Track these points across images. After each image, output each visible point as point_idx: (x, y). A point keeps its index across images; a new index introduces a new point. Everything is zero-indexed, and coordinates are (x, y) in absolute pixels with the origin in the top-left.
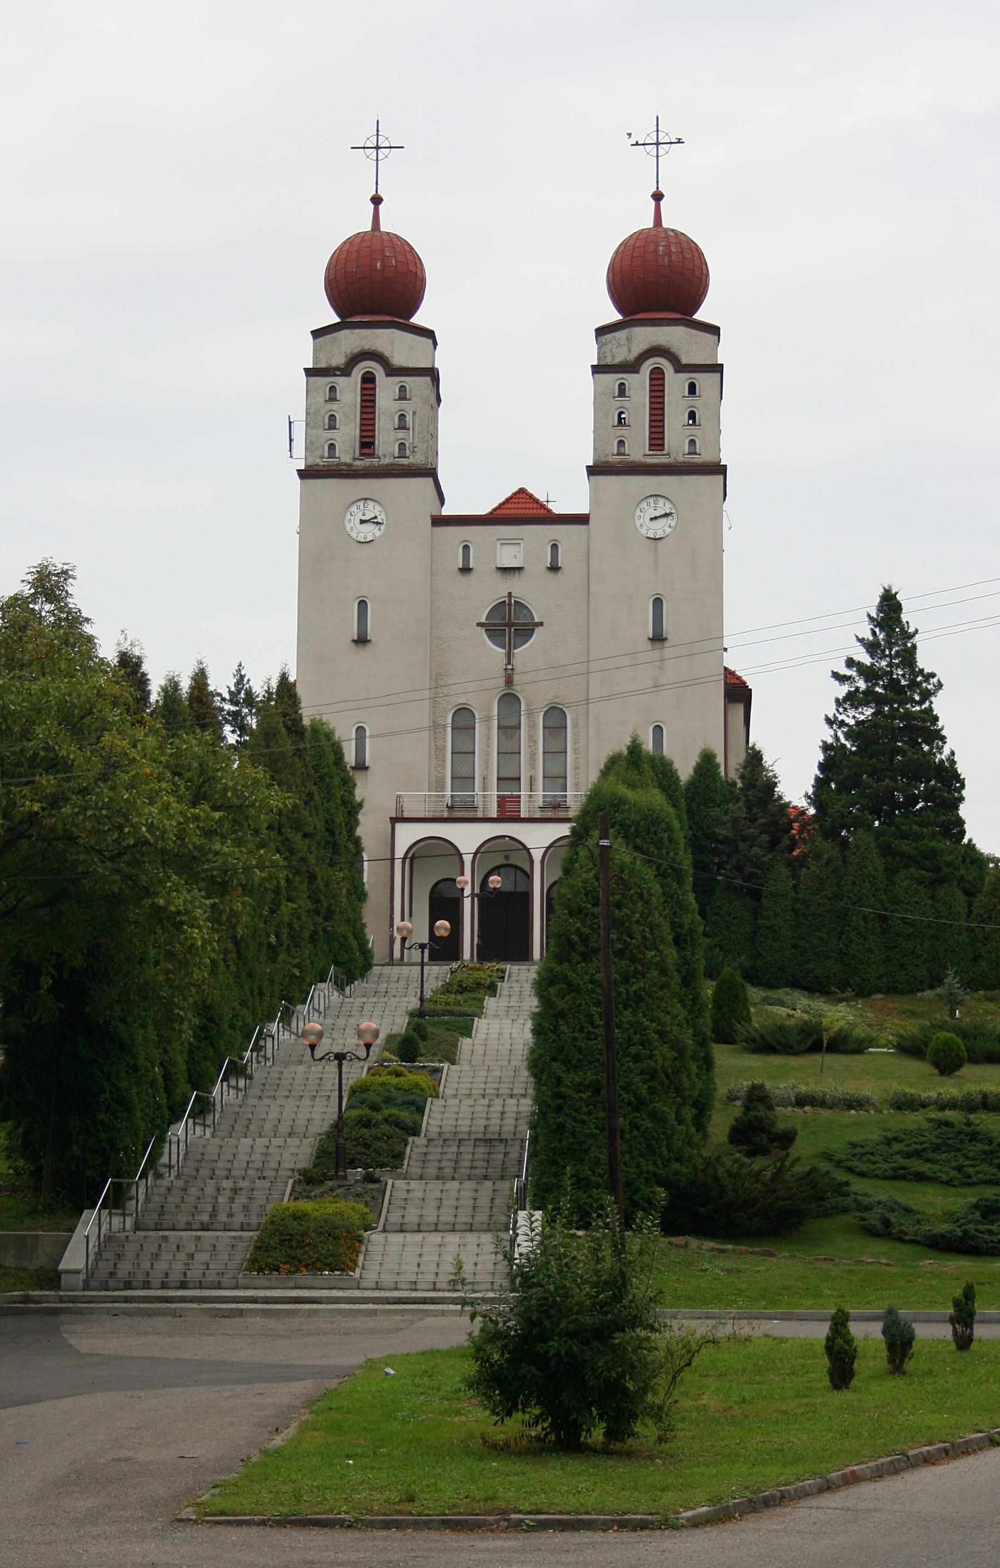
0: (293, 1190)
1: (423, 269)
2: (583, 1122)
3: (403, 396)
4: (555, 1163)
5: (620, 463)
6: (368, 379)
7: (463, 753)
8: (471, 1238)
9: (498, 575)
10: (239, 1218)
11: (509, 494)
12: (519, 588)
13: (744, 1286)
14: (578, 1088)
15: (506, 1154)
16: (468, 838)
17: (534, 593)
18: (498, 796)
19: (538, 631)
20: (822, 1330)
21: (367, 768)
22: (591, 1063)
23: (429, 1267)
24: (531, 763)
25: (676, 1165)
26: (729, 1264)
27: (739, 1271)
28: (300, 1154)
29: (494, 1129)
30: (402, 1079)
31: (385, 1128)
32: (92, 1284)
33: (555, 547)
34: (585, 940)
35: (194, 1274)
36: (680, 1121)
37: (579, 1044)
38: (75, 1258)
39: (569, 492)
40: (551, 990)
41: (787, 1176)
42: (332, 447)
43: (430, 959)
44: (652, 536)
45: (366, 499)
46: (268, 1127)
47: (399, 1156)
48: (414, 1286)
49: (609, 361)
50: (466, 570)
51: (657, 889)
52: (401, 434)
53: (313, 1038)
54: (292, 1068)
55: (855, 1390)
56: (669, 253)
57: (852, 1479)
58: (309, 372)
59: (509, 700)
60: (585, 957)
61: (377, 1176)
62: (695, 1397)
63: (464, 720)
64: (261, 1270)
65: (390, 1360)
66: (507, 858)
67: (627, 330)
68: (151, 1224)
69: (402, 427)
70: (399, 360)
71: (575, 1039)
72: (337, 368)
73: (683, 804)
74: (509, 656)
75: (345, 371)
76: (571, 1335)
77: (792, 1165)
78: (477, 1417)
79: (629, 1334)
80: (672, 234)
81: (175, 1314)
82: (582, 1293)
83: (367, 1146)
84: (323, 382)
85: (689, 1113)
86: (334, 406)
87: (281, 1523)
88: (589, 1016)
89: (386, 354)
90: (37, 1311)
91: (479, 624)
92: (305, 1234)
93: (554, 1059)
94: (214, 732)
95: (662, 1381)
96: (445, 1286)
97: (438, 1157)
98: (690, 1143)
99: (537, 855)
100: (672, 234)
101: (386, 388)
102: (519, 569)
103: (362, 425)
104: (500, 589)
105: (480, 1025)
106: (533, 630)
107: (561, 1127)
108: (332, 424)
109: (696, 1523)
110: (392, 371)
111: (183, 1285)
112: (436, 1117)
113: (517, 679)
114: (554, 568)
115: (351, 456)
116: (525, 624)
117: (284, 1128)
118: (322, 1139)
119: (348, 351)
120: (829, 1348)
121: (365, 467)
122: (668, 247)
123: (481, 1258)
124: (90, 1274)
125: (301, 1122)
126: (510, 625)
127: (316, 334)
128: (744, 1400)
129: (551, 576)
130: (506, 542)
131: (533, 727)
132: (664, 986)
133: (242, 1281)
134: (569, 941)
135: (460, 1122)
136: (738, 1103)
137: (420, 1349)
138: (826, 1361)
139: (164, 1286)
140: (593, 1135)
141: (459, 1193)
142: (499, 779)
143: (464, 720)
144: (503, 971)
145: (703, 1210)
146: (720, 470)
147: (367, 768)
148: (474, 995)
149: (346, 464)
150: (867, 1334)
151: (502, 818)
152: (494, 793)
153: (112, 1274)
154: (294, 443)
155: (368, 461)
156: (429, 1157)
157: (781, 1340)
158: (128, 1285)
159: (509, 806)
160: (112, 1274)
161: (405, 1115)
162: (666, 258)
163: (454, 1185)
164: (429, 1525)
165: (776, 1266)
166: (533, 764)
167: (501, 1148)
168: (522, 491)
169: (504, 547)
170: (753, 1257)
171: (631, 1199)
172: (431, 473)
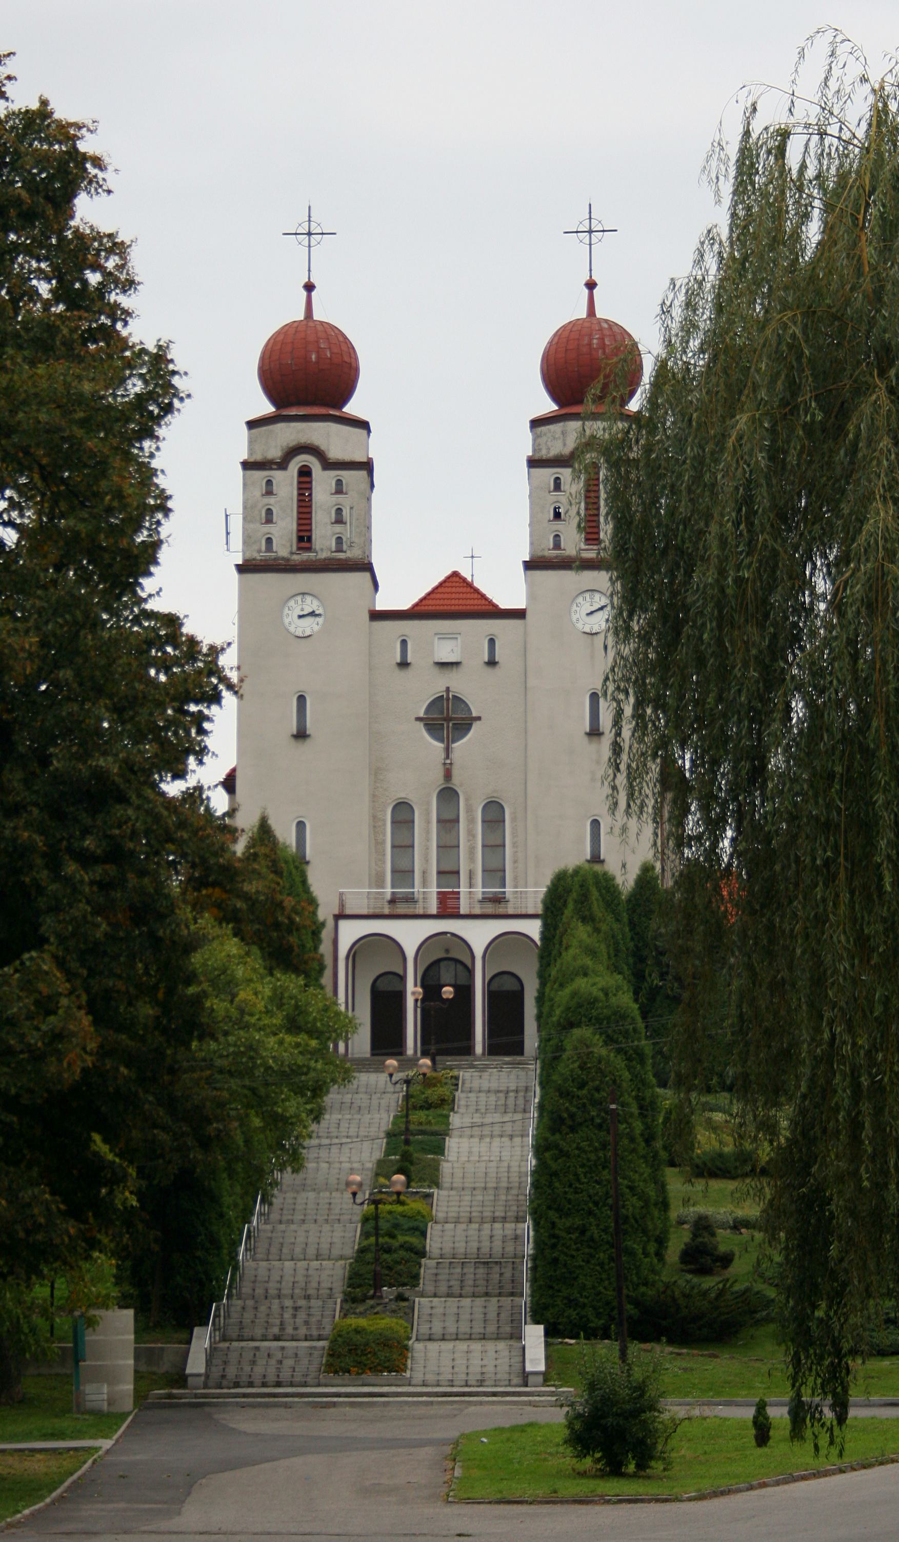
0: (341, 1308)
1: (356, 359)
2: (573, 1257)
3: (339, 489)
4: (551, 1287)
5: (556, 557)
6: (305, 473)
7: (403, 847)
8: (490, 1346)
9: (436, 670)
10: (303, 1331)
11: (442, 578)
12: (458, 683)
13: (696, 1381)
14: (569, 1231)
15: (501, 1274)
16: (410, 935)
17: (471, 686)
18: (439, 893)
19: (476, 726)
20: (749, 1413)
22: (578, 1211)
23: (461, 1368)
24: (471, 857)
25: (643, 1289)
26: (684, 1365)
27: (692, 1370)
28: (333, 1275)
29: (485, 1250)
30: (406, 1207)
31: (402, 1253)
32: (210, 1384)
33: (492, 642)
34: (572, 1116)
35: (285, 1375)
36: (646, 1255)
37: (568, 1196)
38: (196, 1364)
39: (506, 586)
40: (547, 1155)
41: (728, 1296)
42: (269, 541)
44: (588, 631)
45: (303, 594)
46: (298, 1250)
47: (416, 1277)
48: (451, 1383)
49: (544, 454)
50: (404, 664)
51: (627, 1075)
52: (338, 528)
53: (354, 1188)
54: (304, 1195)
55: (771, 1447)
56: (603, 346)
57: (764, 1485)
58: (246, 465)
59: (448, 795)
60: (573, 1129)
61: (406, 1296)
62: (680, 1450)
63: (403, 814)
64: (336, 1372)
65: (485, 1433)
66: (447, 951)
67: (561, 424)
68: (234, 1335)
69: (339, 521)
70: (335, 453)
71: (566, 1193)
72: (276, 463)
73: (625, 917)
74: (448, 750)
75: (282, 465)
76: (617, 1415)
77: (731, 1286)
78: (567, 1460)
79: (648, 1414)
80: (606, 326)
81: (286, 1406)
82: (624, 1393)
83: (390, 1268)
84: (260, 476)
85: (652, 1248)
86: (271, 500)
87: (499, 1502)
88: (576, 1175)
89: (322, 448)
90: (184, 1404)
91: (418, 719)
92: (367, 1344)
93: (549, 1208)
95: (661, 1441)
96: (474, 1383)
97: (446, 1277)
98: (653, 1271)
99: (478, 951)
100: (606, 326)
101: (323, 481)
102: (457, 664)
103: (299, 519)
104: (438, 684)
105: (452, 1144)
106: (471, 725)
107: (555, 1261)
108: (269, 517)
109: (690, 1499)
110: (329, 465)
111: (278, 1384)
112: (437, 1240)
113: (455, 772)
114: (492, 663)
115: (289, 550)
116: (463, 719)
117: (311, 1251)
118: (351, 1264)
119: (285, 444)
120: (755, 1422)
121: (303, 562)
122: (602, 339)
123: (499, 1362)
124: (207, 1376)
125: (325, 1246)
126: (448, 719)
127: (252, 424)
128: (705, 1453)
129: (489, 670)
130: (444, 636)
131: (471, 820)
132: (634, 1150)
133: (323, 1381)
134: (560, 1118)
135: (457, 1245)
136: (686, 1226)
137: (493, 1426)
138: (753, 1432)
139: (264, 1385)
140: (580, 1267)
141: (471, 1309)
142: (439, 873)
143: (403, 814)
144: (457, 1078)
145: (664, 1323)
148: (439, 1111)
149: (283, 558)
150: (779, 1414)
151: (442, 915)
152: (434, 890)
153: (223, 1377)
154: (231, 536)
155: (305, 556)
156: (440, 1277)
157: (726, 1419)
158: (237, 1385)
159: (450, 903)
160: (223, 1377)
161: (413, 1240)
162: (600, 352)
163: (466, 1302)
164: (567, 1502)
165: (721, 1365)
166: (472, 859)
167: (496, 1269)
168: (455, 574)
169: (442, 642)
170: (701, 1359)
171: (610, 1316)
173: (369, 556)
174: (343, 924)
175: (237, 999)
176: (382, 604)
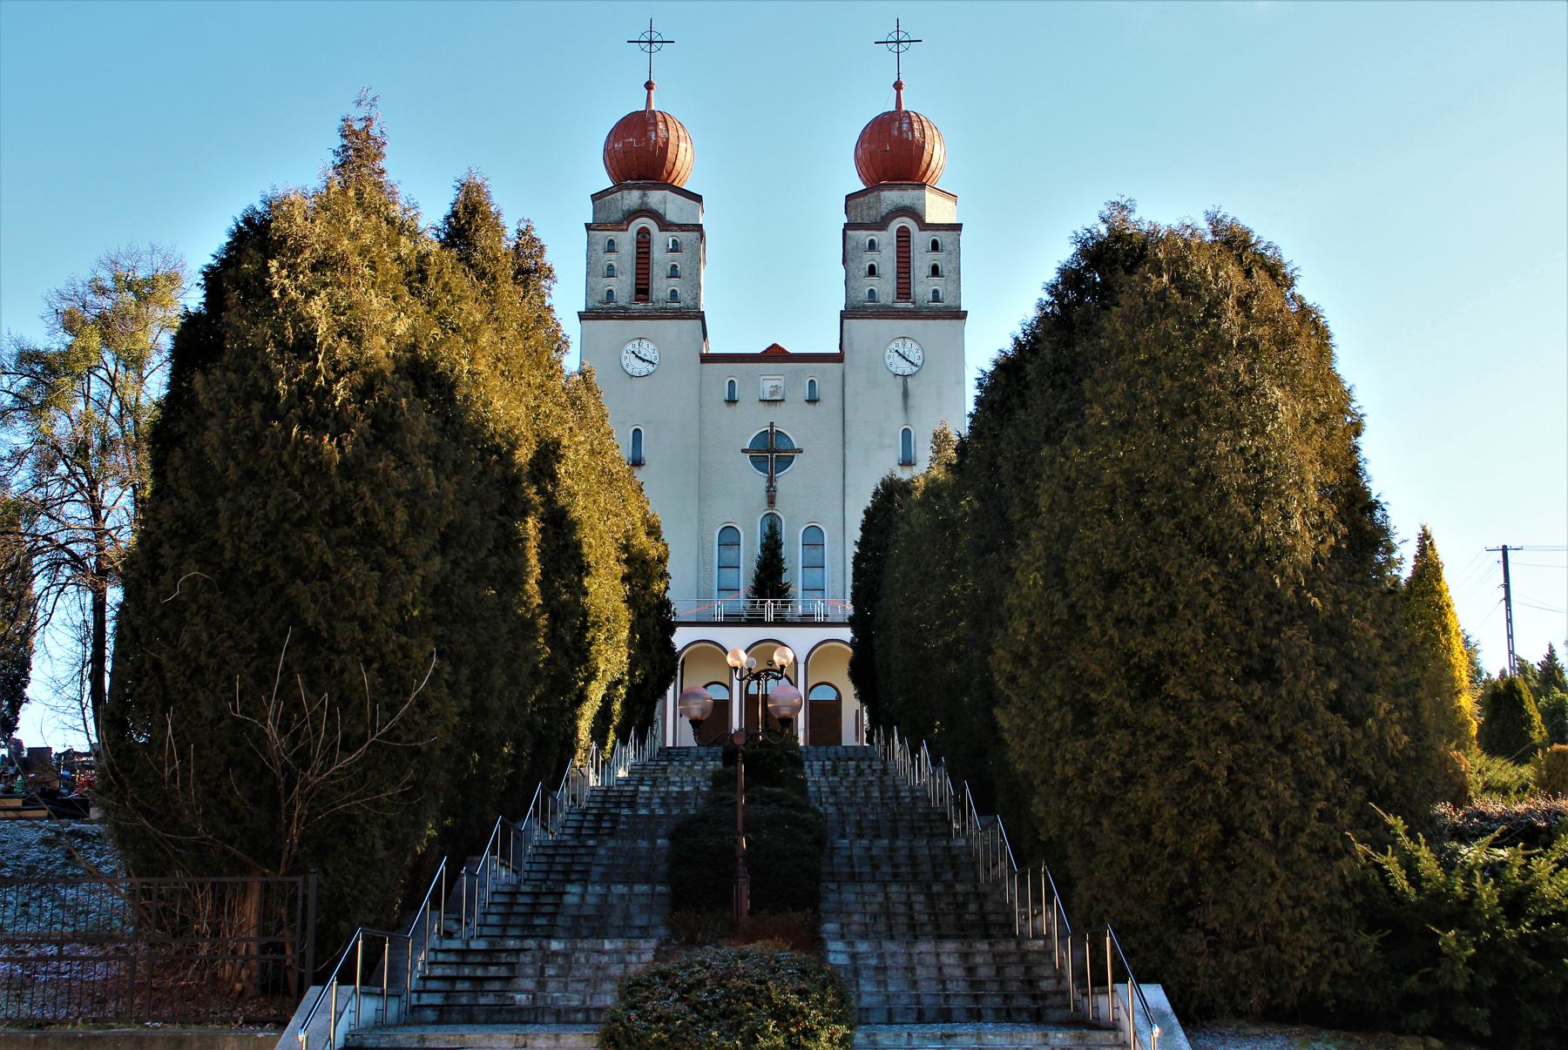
17: (793, 423)
43: (758, 903)
58: (588, 227)
70: (672, 216)
74: (771, 480)
94: (1445, 923)
110: (665, 225)
127: (595, 197)
129: (810, 407)
143: (729, 538)
146: (960, 315)
168: (775, 346)
173: (697, 297)
175: (64, 446)
176: (715, 346)
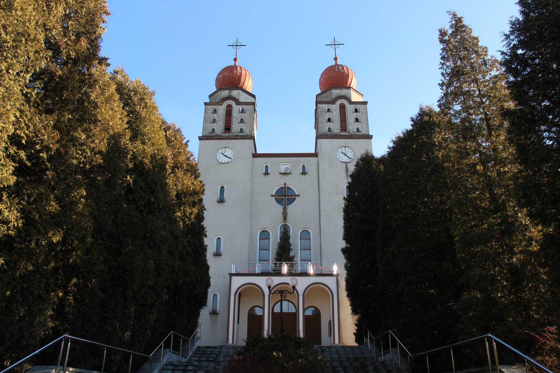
17: (295, 183)
21: (218, 314)
74: (285, 209)
86: (216, 115)
106: (295, 199)
110: (238, 103)
129: (303, 176)
143: (265, 235)
147: (218, 314)
155: (227, 134)
172: (252, 138)
174: (234, 278)
